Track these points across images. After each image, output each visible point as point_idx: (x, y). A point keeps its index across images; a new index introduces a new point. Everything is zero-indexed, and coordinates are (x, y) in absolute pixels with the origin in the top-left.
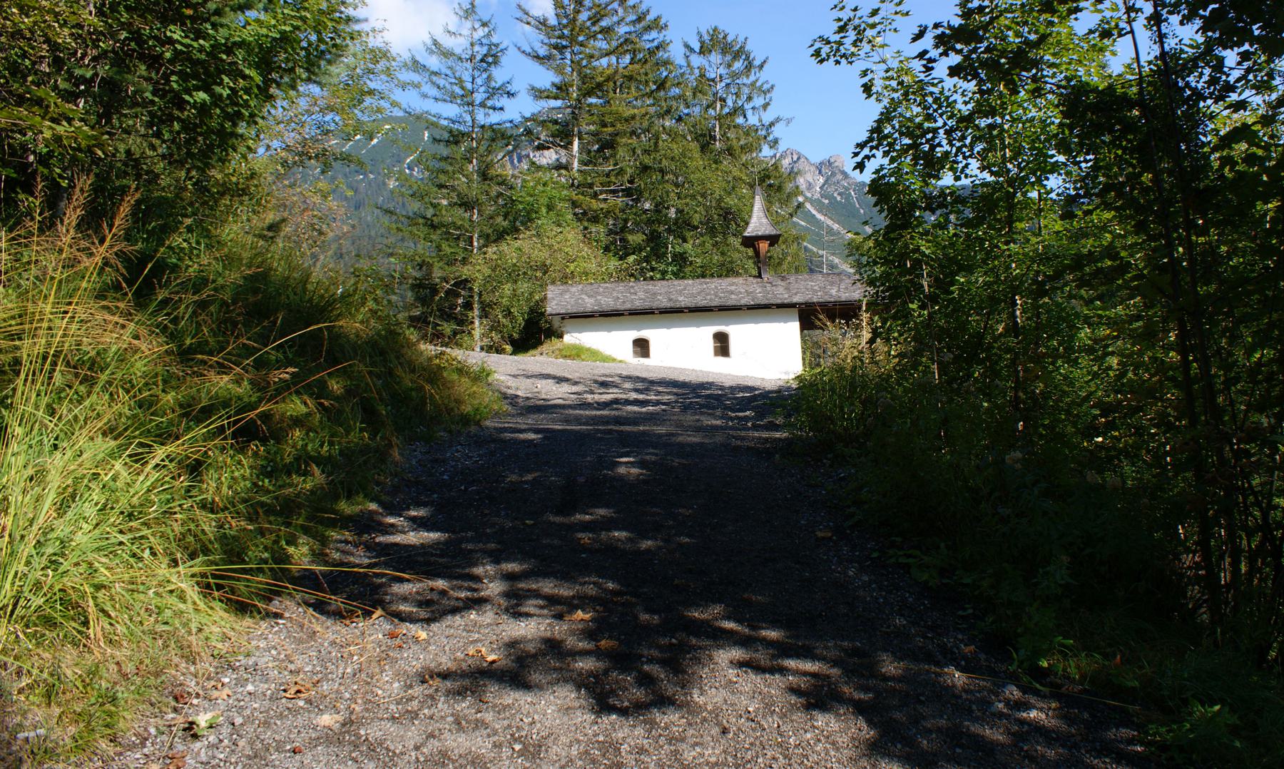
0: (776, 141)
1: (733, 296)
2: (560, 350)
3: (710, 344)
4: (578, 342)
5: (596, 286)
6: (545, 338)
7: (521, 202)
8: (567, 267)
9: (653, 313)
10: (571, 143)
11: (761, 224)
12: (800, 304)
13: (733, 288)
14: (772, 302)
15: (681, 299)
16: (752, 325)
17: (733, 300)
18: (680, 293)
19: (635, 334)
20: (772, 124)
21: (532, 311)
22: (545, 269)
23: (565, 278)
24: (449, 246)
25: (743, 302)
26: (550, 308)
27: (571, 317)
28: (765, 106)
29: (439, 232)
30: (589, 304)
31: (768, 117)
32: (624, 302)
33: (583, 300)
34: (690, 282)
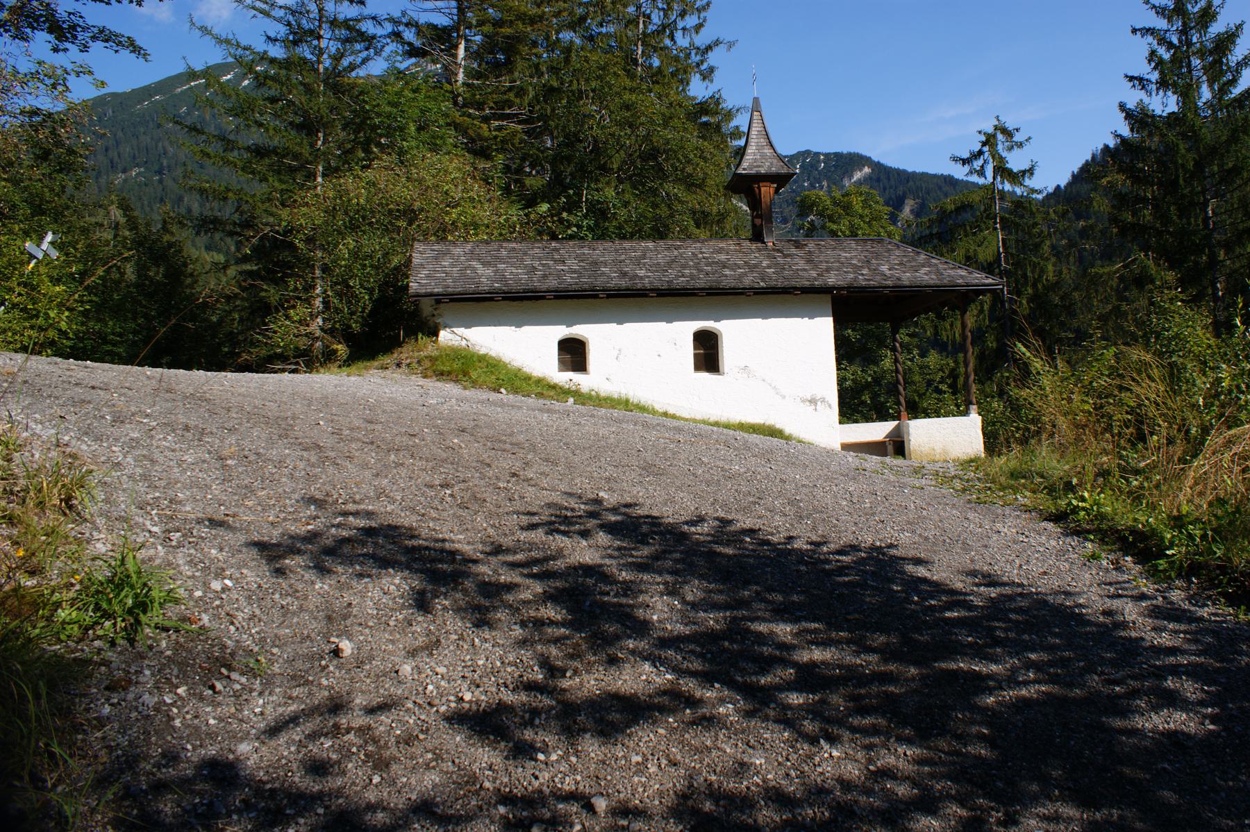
0: (712, 70)
1: (727, 272)
2: (432, 359)
3: (688, 352)
4: (464, 343)
5: (495, 246)
6: (407, 335)
7: (379, 115)
8: (448, 213)
9: (596, 297)
10: (456, 47)
11: (763, 156)
12: (839, 288)
13: (723, 257)
14: (793, 283)
15: (642, 273)
16: (759, 321)
17: (729, 277)
18: (638, 262)
19: (562, 331)
20: (709, 48)
21: (384, 285)
22: (410, 214)
23: (442, 233)
24: (280, 181)
25: (747, 282)
26: (418, 283)
27: (452, 300)
28: (698, 28)
29: (267, 161)
30: (485, 276)
31: (701, 40)
32: (545, 276)
33: (474, 269)
34: (650, 245)
